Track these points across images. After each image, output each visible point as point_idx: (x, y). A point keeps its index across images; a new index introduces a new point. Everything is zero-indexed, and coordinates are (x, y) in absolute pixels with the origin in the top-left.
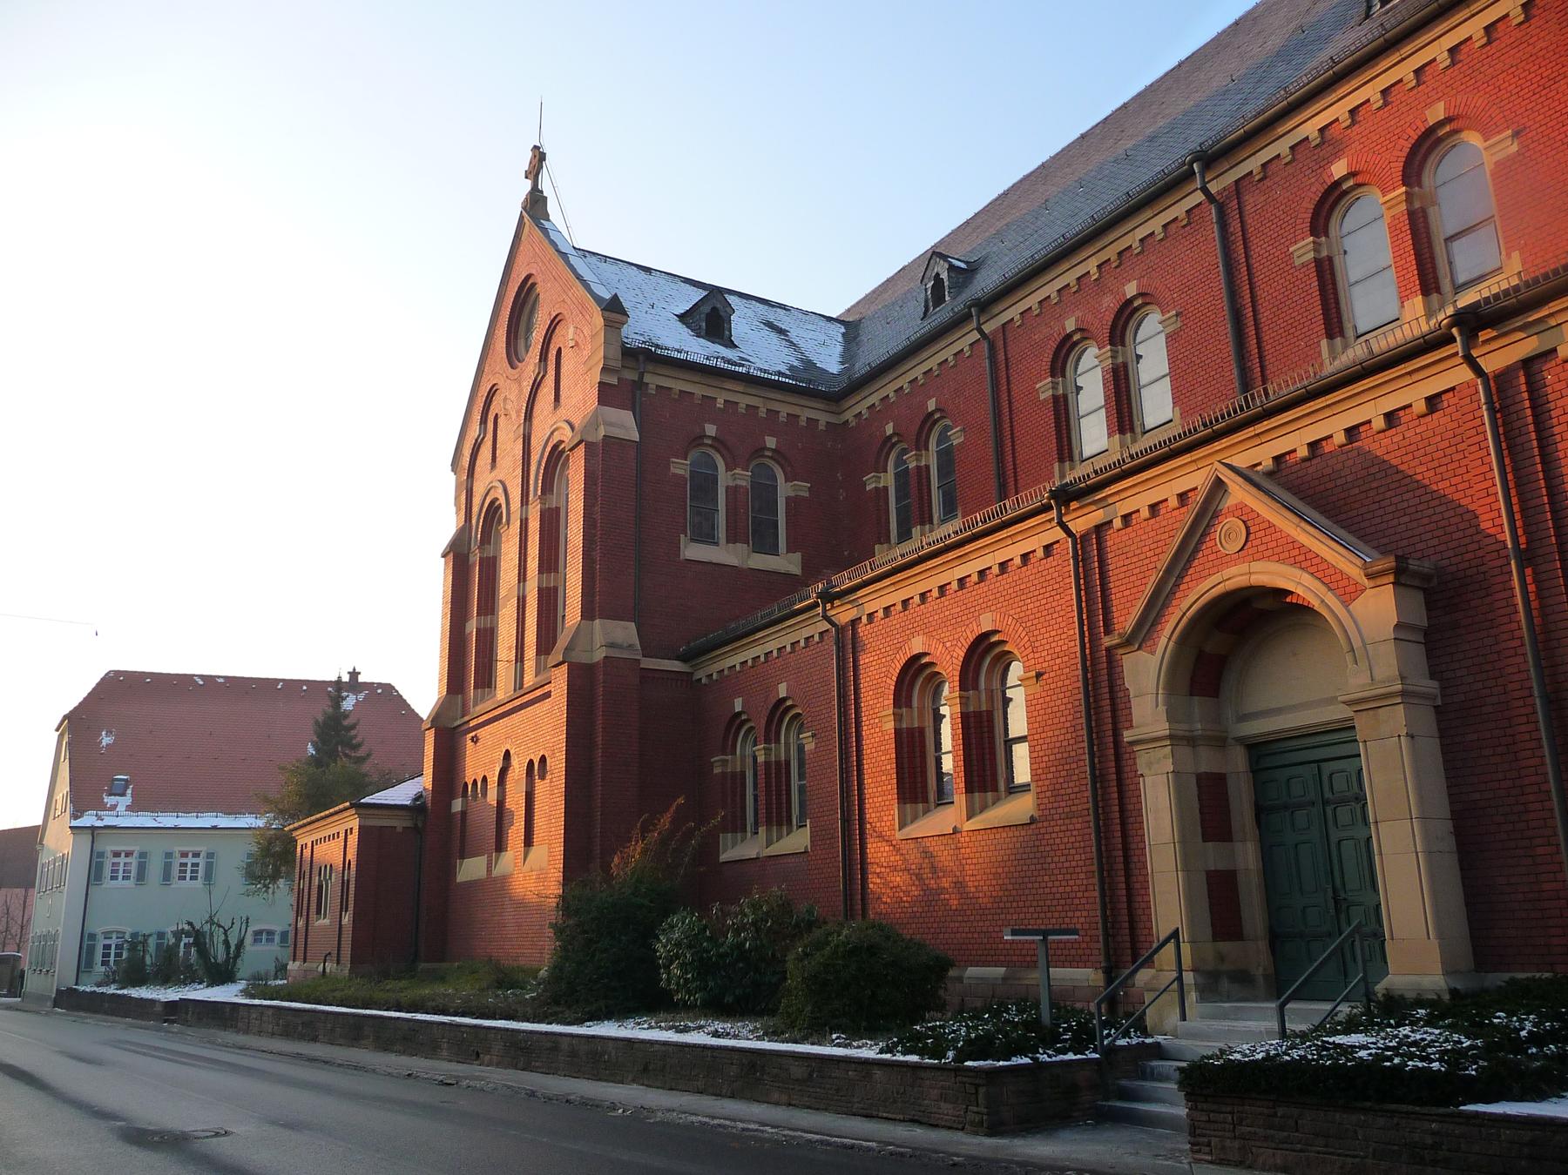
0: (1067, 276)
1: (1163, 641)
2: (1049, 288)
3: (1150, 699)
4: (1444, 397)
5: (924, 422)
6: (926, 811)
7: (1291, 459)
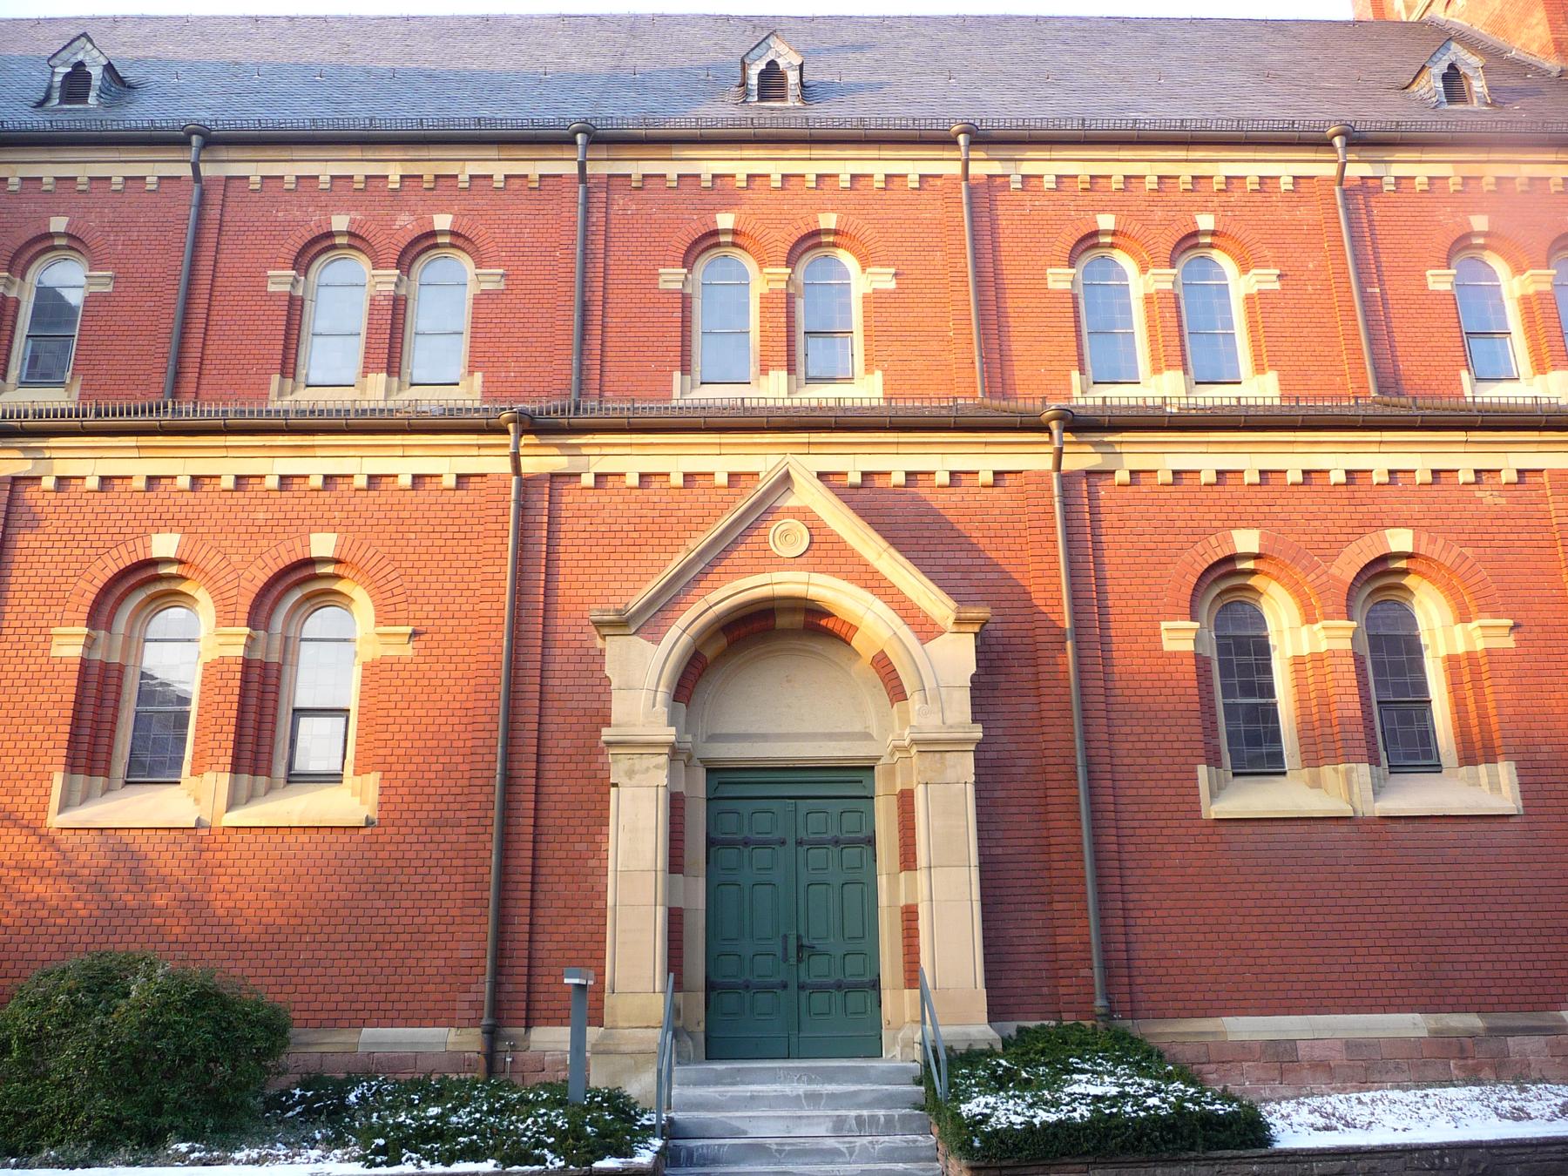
0: (358, 166)
1: (673, 632)
2: (324, 167)
3: (644, 697)
4: (472, 479)
5: (418, 240)
6: (107, 790)
7: (879, 482)
